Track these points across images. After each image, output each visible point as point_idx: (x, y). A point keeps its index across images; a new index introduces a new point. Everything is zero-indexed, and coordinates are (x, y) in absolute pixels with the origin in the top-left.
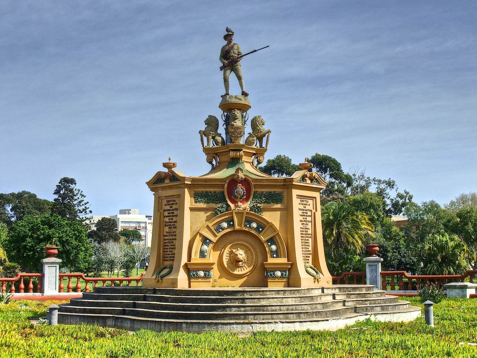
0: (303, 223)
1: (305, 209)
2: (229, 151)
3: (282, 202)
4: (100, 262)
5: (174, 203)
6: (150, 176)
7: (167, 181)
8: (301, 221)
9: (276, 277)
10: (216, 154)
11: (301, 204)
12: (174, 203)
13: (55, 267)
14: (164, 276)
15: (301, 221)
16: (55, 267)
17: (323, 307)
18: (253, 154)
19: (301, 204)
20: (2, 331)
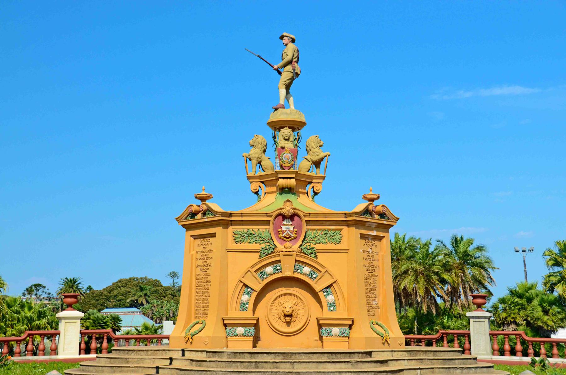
0: (369, 268)
1: (206, 250)
2: (277, 179)
3: (341, 242)
4: (415, 284)
5: (208, 243)
6: (181, 210)
7: (199, 216)
8: (365, 266)
9: (464, 346)
10: (263, 182)
11: (366, 245)
12: (208, 243)
13: (168, 339)
14: (195, 333)
15: (365, 266)
16: (327, 273)
17: (124, 334)
18: (308, 183)
19: (366, 245)
20: (297, 62)
